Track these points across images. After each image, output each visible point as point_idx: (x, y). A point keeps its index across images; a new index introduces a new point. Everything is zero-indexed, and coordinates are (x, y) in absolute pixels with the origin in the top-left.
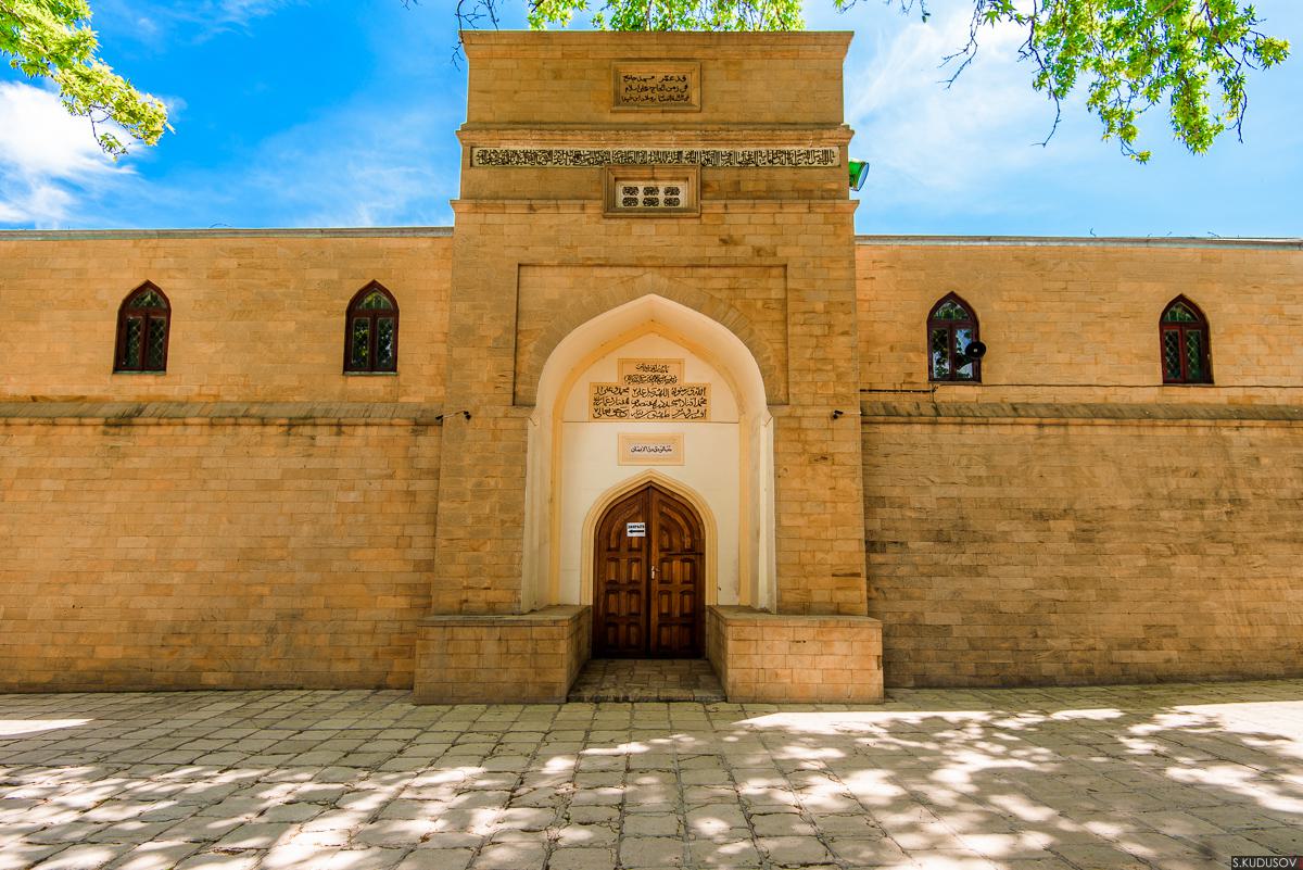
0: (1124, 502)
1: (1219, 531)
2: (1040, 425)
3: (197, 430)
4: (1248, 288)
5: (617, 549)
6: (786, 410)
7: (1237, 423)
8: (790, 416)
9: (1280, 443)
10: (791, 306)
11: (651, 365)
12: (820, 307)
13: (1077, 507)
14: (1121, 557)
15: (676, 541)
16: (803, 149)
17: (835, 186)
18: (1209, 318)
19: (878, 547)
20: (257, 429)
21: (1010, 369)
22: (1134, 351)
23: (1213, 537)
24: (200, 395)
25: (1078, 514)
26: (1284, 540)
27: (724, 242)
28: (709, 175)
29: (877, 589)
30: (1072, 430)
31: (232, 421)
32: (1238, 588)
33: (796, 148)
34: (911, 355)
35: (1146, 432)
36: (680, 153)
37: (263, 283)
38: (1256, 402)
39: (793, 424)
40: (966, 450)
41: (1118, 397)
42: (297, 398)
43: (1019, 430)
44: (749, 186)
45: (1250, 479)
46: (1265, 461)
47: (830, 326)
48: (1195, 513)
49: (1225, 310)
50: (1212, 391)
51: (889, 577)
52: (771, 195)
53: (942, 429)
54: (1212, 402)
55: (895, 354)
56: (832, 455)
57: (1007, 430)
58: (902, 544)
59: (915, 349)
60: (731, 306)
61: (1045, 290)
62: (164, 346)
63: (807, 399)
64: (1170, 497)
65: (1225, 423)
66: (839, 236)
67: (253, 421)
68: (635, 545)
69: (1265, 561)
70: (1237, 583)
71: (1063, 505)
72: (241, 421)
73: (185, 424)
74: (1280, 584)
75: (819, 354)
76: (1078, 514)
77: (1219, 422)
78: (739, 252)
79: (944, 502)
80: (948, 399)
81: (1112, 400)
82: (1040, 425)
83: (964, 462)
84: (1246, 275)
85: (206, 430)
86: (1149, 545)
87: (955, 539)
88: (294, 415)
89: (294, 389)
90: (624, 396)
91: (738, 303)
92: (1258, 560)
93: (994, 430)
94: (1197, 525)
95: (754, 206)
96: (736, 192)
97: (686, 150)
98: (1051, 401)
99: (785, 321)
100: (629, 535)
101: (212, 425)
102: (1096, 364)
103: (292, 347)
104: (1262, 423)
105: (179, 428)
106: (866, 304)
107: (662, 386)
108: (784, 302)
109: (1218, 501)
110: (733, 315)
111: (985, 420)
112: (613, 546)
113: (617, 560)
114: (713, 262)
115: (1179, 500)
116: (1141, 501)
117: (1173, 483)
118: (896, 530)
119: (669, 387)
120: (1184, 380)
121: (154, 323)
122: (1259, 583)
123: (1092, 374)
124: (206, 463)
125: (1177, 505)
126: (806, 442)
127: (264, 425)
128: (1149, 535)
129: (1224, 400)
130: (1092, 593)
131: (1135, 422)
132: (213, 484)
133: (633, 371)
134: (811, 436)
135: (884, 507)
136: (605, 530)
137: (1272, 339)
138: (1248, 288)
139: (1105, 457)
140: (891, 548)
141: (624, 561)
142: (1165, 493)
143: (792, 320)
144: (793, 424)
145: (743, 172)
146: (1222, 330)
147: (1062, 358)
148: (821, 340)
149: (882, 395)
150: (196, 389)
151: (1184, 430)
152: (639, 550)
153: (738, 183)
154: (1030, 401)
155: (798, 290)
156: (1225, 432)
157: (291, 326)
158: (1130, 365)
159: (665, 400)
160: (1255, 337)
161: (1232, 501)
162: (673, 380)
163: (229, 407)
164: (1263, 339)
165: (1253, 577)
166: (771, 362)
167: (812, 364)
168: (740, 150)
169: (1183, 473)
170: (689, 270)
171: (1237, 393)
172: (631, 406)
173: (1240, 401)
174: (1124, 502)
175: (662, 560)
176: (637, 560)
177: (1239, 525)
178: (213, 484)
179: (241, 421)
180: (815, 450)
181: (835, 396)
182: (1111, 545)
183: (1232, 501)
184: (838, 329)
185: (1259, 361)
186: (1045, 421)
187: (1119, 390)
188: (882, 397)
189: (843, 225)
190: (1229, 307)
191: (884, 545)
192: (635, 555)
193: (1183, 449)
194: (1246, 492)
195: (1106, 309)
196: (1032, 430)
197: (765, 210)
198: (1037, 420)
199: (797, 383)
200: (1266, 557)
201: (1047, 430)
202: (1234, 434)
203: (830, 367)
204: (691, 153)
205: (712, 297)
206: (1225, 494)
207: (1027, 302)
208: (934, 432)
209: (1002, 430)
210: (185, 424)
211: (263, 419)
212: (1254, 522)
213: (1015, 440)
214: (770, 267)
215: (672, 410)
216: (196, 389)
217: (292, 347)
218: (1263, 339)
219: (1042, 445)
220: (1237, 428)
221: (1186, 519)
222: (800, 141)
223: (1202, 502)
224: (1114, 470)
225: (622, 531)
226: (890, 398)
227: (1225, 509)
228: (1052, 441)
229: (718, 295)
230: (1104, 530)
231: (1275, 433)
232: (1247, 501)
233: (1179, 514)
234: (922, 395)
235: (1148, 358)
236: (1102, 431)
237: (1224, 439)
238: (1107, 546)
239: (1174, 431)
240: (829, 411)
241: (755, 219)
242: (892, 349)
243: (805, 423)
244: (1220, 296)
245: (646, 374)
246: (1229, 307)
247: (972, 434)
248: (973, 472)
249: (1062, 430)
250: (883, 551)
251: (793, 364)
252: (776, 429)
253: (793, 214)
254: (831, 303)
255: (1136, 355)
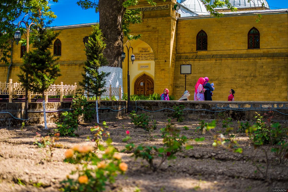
0: (229, 77)
1: (248, 83)
2: (216, 60)
3: (66, 66)
4: (270, 24)
5: (139, 88)
6: (157, 60)
7: (260, 58)
8: (158, 62)
9: (269, 63)
10: (159, 39)
11: (144, 48)
12: (164, 39)
13: (219, 78)
14: (226, 89)
15: (150, 86)
16: (163, 6)
17: (168, 13)
18: (247, 34)
19: (178, 87)
20: (75, 66)
21: (214, 47)
22: (241, 41)
23: (247, 85)
24: (66, 60)
25: (219, 80)
26: (262, 85)
27: (147, 27)
28: (145, 13)
29: (176, 95)
30: (223, 61)
31: (71, 65)
32: (249, 95)
33: (161, 5)
34: (193, 45)
35: (239, 61)
36: (140, 8)
37: (75, 37)
38: (270, 52)
39: (158, 63)
40: (200, 66)
41: (237, 52)
42: (81, 60)
43: (212, 61)
44: (152, 15)
45: (259, 71)
46: (264, 67)
47: (166, 43)
48: (244, 79)
49: (264, 30)
50: (259, 50)
51: (179, 93)
52: (156, 17)
53: (195, 62)
54: (259, 53)
55: (189, 45)
56: (165, 69)
57: (209, 61)
58: (183, 86)
59: (194, 43)
60: (149, 40)
61: (222, 28)
62: (61, 50)
63: (161, 58)
64: (240, 76)
65: (257, 58)
66: (168, 24)
67: (74, 65)
68: (142, 87)
69: (257, 90)
70: (249, 94)
71: (216, 78)
72: (72, 65)
73: (64, 66)
74: (258, 95)
75: (164, 49)
76: (219, 80)
77: (256, 58)
78: (150, 29)
79: (193, 78)
80: (200, 54)
81: (236, 53)
82: (216, 60)
83: (199, 69)
84: (270, 21)
85: (67, 66)
86: (232, 86)
87: (193, 85)
88: (80, 63)
89: (81, 58)
90: (139, 56)
91: (150, 39)
92: (255, 89)
93: (206, 61)
94: (244, 82)
95: (152, 19)
96: (150, 17)
97: (141, 8)
98: (222, 54)
99: (158, 42)
100: (141, 85)
101: (68, 66)
102: (233, 45)
103: (80, 50)
104: (266, 58)
105: (63, 66)
106: (184, 34)
107: (147, 53)
108: (158, 38)
109: (250, 76)
110: (149, 41)
111: (204, 59)
112: (138, 87)
113: (139, 90)
114: (145, 31)
115: (242, 76)
116: (233, 77)
117: (241, 72)
118: (182, 83)
119: (148, 53)
120: (254, 48)
121: (59, 46)
122: (254, 94)
123: (231, 47)
124: (68, 73)
125: (241, 77)
126: (160, 67)
127: (76, 65)
128: (233, 84)
129: (262, 52)
130: (218, 96)
131: (236, 59)
132: (69, 77)
133: (141, 50)
134: (161, 65)
135: (181, 79)
136: (136, 84)
137: (275, 37)
138: (270, 24)
139: (228, 67)
140: (180, 87)
141: (140, 91)
142: (239, 74)
143: (159, 42)
144: (158, 63)
145: (151, 12)
146: (263, 35)
147: (225, 44)
148: (164, 46)
149: (186, 54)
150: (66, 58)
151: (248, 60)
152: (143, 88)
153: (150, 14)
154: (218, 54)
155: (160, 36)
156: (257, 60)
157: (80, 45)
158: (240, 45)
159: (147, 56)
160: (271, 36)
161: (253, 76)
162: (149, 51)
163: (71, 62)
164: (273, 37)
165: (253, 93)
166: (155, 51)
167: (162, 51)
168: (151, 7)
169: (244, 70)
170: (142, 33)
171: (265, 50)
172: (141, 57)
173: (266, 52)
174: (229, 77)
175: (147, 90)
176: (143, 90)
177: (253, 82)
178: (69, 77)
179: (72, 65)
180: (162, 68)
181: (166, 57)
182: (224, 86)
183: (253, 76)
184: (167, 44)
185: (271, 42)
186: (217, 59)
187: (237, 51)
188: (186, 54)
189: (169, 21)
190: (265, 29)
191: (179, 86)
192: (142, 89)
193: (246, 65)
194: (257, 74)
195: (235, 32)
196: (214, 61)
197: (155, 19)
198: (215, 59)
199: (159, 55)
200: (257, 89)
201: (217, 61)
202: (259, 60)
203: (165, 51)
204: (142, 8)
205: (145, 38)
206: (252, 75)
207: (218, 31)
208: (194, 62)
209: (208, 61)
210: (64, 66)
211: (76, 64)
212: (257, 81)
213: (210, 64)
214: (156, 31)
215: (148, 58)
216: (66, 58)
217: (80, 50)
218: (273, 37)
219: (216, 64)
220: (260, 59)
221: (242, 80)
222: (162, 4)
223: (247, 77)
224: (229, 70)
225: (140, 84)
226: (188, 54)
227: (251, 78)
228: (218, 64)
229: (146, 37)
230: (224, 83)
231: (269, 60)
232: (257, 76)
233: (241, 79)
234: (195, 54)
235: (245, 43)
236: (229, 61)
237: (256, 62)
238: (223, 86)
239: (245, 60)
240: (164, 60)
241: (153, 22)
242: (189, 43)
243: (160, 63)
244: (263, 27)
245: (143, 50)
246: (265, 29)
247: (202, 62)
248: (200, 71)
249: (220, 61)
250: (179, 88)
251: (159, 51)
252: (155, 64)
253: (160, 20)
254: (166, 38)
255: (242, 42)
